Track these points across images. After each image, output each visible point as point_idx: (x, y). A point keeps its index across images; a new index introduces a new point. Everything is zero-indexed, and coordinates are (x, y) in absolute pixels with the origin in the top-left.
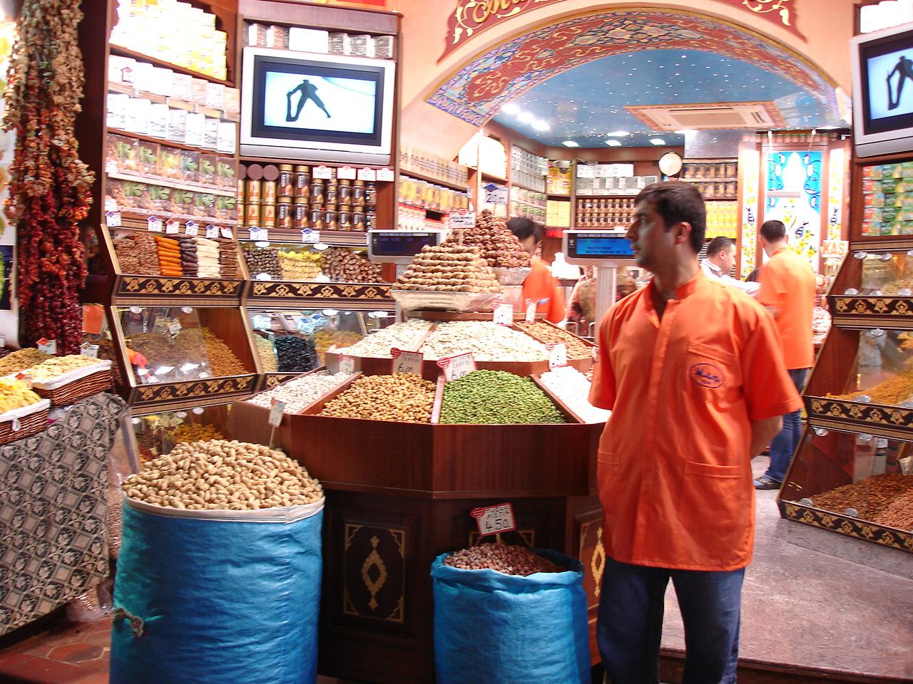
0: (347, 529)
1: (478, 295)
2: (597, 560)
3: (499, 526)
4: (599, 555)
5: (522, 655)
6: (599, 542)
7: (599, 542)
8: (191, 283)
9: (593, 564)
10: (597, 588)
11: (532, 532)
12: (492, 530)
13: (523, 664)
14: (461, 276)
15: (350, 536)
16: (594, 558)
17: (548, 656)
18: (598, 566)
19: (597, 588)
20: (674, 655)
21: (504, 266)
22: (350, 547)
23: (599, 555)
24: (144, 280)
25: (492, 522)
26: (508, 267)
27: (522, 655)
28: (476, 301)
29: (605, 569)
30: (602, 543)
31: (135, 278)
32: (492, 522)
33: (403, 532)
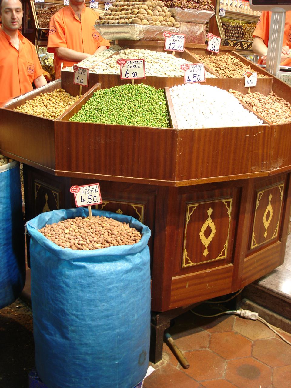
0: (35, 186)
1: (148, 26)
2: (267, 215)
3: (90, 200)
4: (269, 211)
5: (81, 311)
6: (270, 203)
7: (270, 203)
8: (241, 43)
9: (264, 218)
10: (266, 232)
11: (142, 207)
12: (85, 203)
13: (81, 317)
14: (136, 12)
15: (37, 191)
16: (266, 214)
17: (102, 312)
18: (267, 219)
19: (266, 232)
20: (283, 299)
21: (177, 6)
22: (37, 198)
23: (269, 211)
24: (250, 43)
25: (85, 197)
26: (182, 8)
27: (81, 311)
28: (147, 31)
29: (271, 221)
30: (271, 204)
31: (246, 42)
32: (85, 197)
33: (58, 194)
